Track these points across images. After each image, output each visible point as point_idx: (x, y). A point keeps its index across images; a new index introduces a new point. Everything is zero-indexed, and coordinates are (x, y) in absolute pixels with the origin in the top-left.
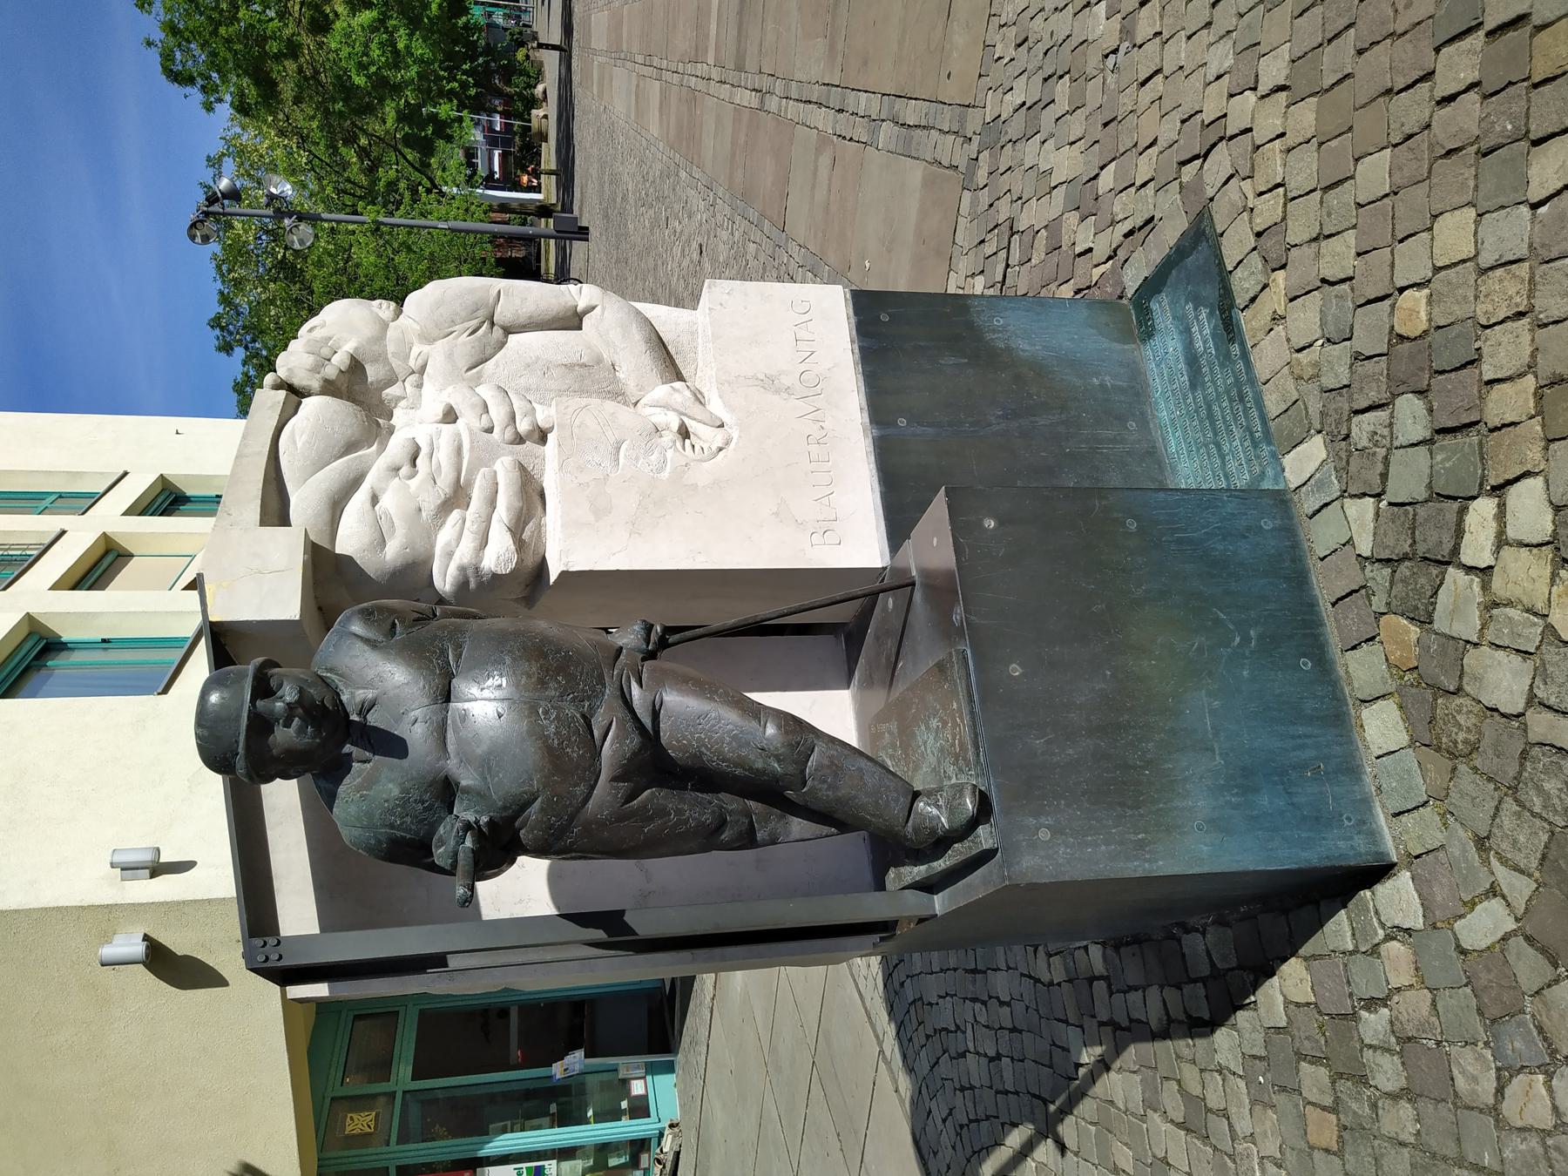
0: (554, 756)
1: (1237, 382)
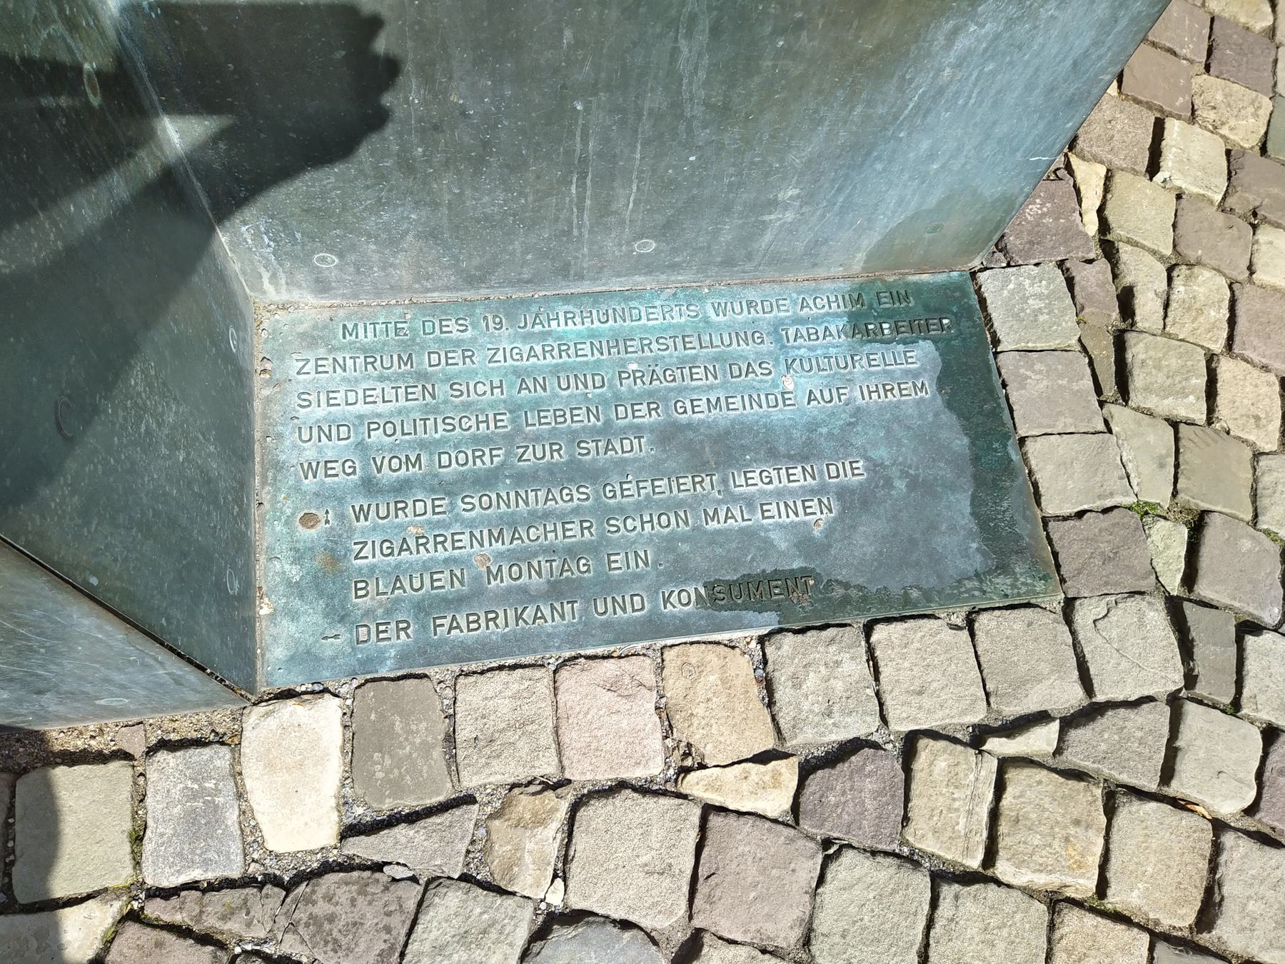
1: (607, 586)
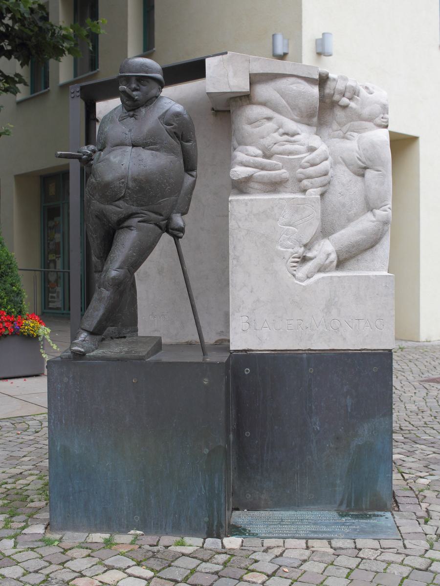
0: (107, 185)
